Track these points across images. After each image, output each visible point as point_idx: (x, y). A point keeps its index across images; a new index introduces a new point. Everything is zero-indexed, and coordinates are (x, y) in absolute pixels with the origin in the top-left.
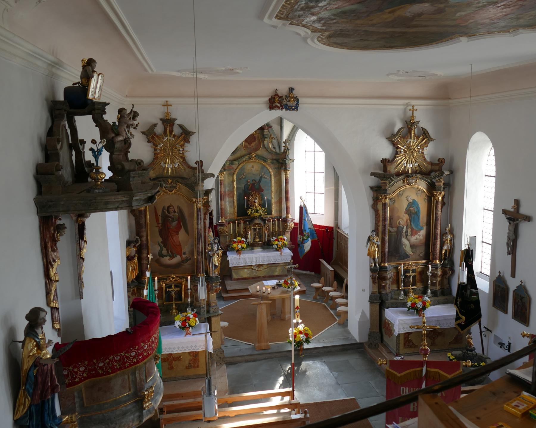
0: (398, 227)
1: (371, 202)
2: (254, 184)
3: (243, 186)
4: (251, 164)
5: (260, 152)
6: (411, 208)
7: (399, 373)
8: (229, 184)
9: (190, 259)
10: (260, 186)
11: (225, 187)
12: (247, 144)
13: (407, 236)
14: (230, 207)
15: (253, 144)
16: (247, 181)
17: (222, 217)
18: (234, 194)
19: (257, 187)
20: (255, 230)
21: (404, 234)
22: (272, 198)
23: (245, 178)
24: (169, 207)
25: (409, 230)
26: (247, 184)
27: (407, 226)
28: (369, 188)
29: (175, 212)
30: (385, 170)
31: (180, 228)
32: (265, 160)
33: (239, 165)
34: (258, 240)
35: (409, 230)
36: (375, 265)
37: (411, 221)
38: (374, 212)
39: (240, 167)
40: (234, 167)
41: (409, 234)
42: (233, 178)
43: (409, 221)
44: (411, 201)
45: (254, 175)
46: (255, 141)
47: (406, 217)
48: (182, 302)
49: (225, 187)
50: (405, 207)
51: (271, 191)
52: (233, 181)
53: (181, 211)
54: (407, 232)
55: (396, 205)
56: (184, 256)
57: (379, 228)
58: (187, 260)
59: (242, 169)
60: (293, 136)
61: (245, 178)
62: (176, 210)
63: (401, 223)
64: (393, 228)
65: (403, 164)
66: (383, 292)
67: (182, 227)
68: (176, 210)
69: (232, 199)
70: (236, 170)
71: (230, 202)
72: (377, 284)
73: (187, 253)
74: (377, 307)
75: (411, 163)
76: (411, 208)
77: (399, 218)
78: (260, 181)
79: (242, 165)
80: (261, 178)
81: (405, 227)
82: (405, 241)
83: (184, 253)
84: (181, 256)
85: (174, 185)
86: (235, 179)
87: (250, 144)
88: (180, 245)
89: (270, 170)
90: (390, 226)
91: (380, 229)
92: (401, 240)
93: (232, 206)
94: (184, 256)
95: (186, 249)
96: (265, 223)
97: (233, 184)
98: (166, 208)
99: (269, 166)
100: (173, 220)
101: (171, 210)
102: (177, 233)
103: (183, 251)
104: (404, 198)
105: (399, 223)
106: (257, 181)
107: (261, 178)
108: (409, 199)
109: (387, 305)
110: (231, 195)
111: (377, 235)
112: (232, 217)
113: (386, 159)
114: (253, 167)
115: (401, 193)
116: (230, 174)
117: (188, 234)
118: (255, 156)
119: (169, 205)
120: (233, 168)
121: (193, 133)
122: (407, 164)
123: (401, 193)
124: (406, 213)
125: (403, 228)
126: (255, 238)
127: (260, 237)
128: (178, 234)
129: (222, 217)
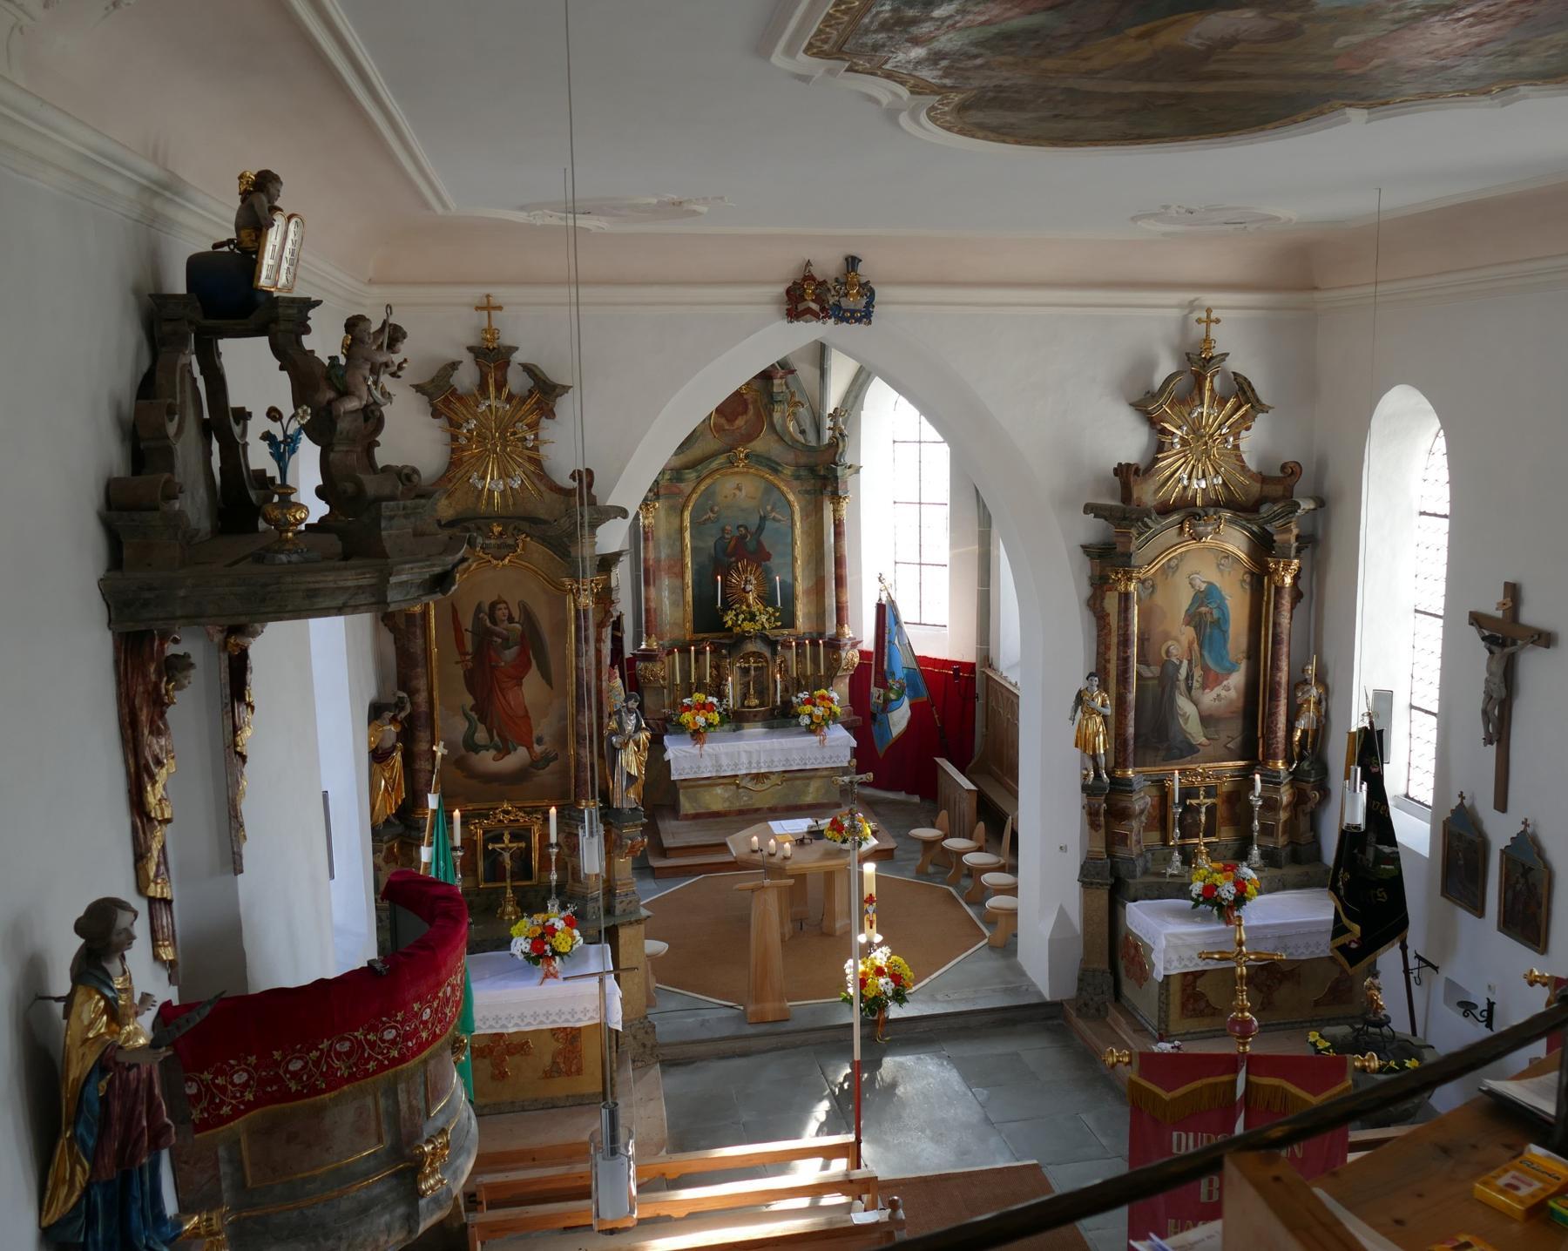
0: (1164, 665)
1: (1086, 591)
2: (743, 537)
3: (711, 543)
4: (735, 480)
5: (760, 445)
6: (1203, 609)
7: (1168, 1090)
8: (669, 537)
9: (555, 758)
10: (759, 543)
11: (657, 547)
12: (723, 421)
13: (1189, 689)
14: (674, 604)
15: (740, 422)
16: (723, 530)
17: (649, 635)
18: (683, 566)
19: (752, 546)
20: (746, 671)
21: (1182, 685)
22: (795, 579)
23: (718, 519)
24: (493, 606)
25: (1198, 673)
26: (722, 538)
27: (1190, 662)
28: (1080, 550)
29: (511, 619)
30: (1126, 495)
31: (528, 666)
32: (774, 467)
33: (699, 484)
34: (755, 702)
35: (1198, 673)
36: (1098, 776)
37: (1201, 646)
38: (1094, 620)
39: (702, 487)
40: (686, 487)
41: (1196, 685)
42: (682, 521)
43: (1196, 646)
44: (1203, 586)
45: (743, 510)
46: (745, 412)
47: (1189, 633)
48: (534, 882)
49: (657, 547)
50: (1185, 606)
51: (794, 559)
52: (681, 530)
53: (528, 617)
54: (1189, 677)
55: (1159, 599)
56: (538, 749)
57: (1108, 666)
58: (546, 759)
59: (709, 494)
60: (856, 397)
61: (718, 519)
62: (516, 614)
63: (1173, 651)
64: (1148, 665)
65: (1180, 480)
66: (1121, 852)
67: (534, 663)
68: (516, 614)
69: (678, 582)
70: (690, 496)
71: (672, 591)
72: (1102, 832)
73: (547, 739)
74: (1103, 896)
75: (1204, 476)
76: (1203, 609)
77: (1167, 636)
78: (761, 528)
79: (708, 481)
80: (763, 519)
81: (1185, 662)
82: (1184, 704)
83: (540, 741)
84: (530, 748)
85: (510, 541)
86: (687, 523)
87: (730, 421)
88: (526, 716)
89: (791, 497)
90: (1142, 659)
91: (1113, 668)
92: (1172, 701)
93: (678, 602)
94: (538, 749)
95: (544, 727)
96: (774, 653)
97: (682, 539)
98: (487, 609)
99: (788, 484)
100: (507, 644)
101: (501, 613)
102: (518, 681)
103: (536, 733)
104: (1181, 580)
105: (1168, 652)
106: (753, 529)
107: (763, 519)
108: (1198, 582)
109: (1132, 891)
110: (677, 570)
111: (1104, 686)
112: (677, 633)
113: (1128, 465)
114: (739, 488)
115: (1173, 563)
116: (672, 508)
117: (549, 683)
118: (747, 456)
119: (495, 598)
120: (680, 492)
121: (566, 389)
122: (1190, 478)
123: (1173, 563)
124: (1188, 624)
125: (1178, 668)
126: (745, 696)
127: (762, 693)
128: (520, 684)
129: (649, 635)
